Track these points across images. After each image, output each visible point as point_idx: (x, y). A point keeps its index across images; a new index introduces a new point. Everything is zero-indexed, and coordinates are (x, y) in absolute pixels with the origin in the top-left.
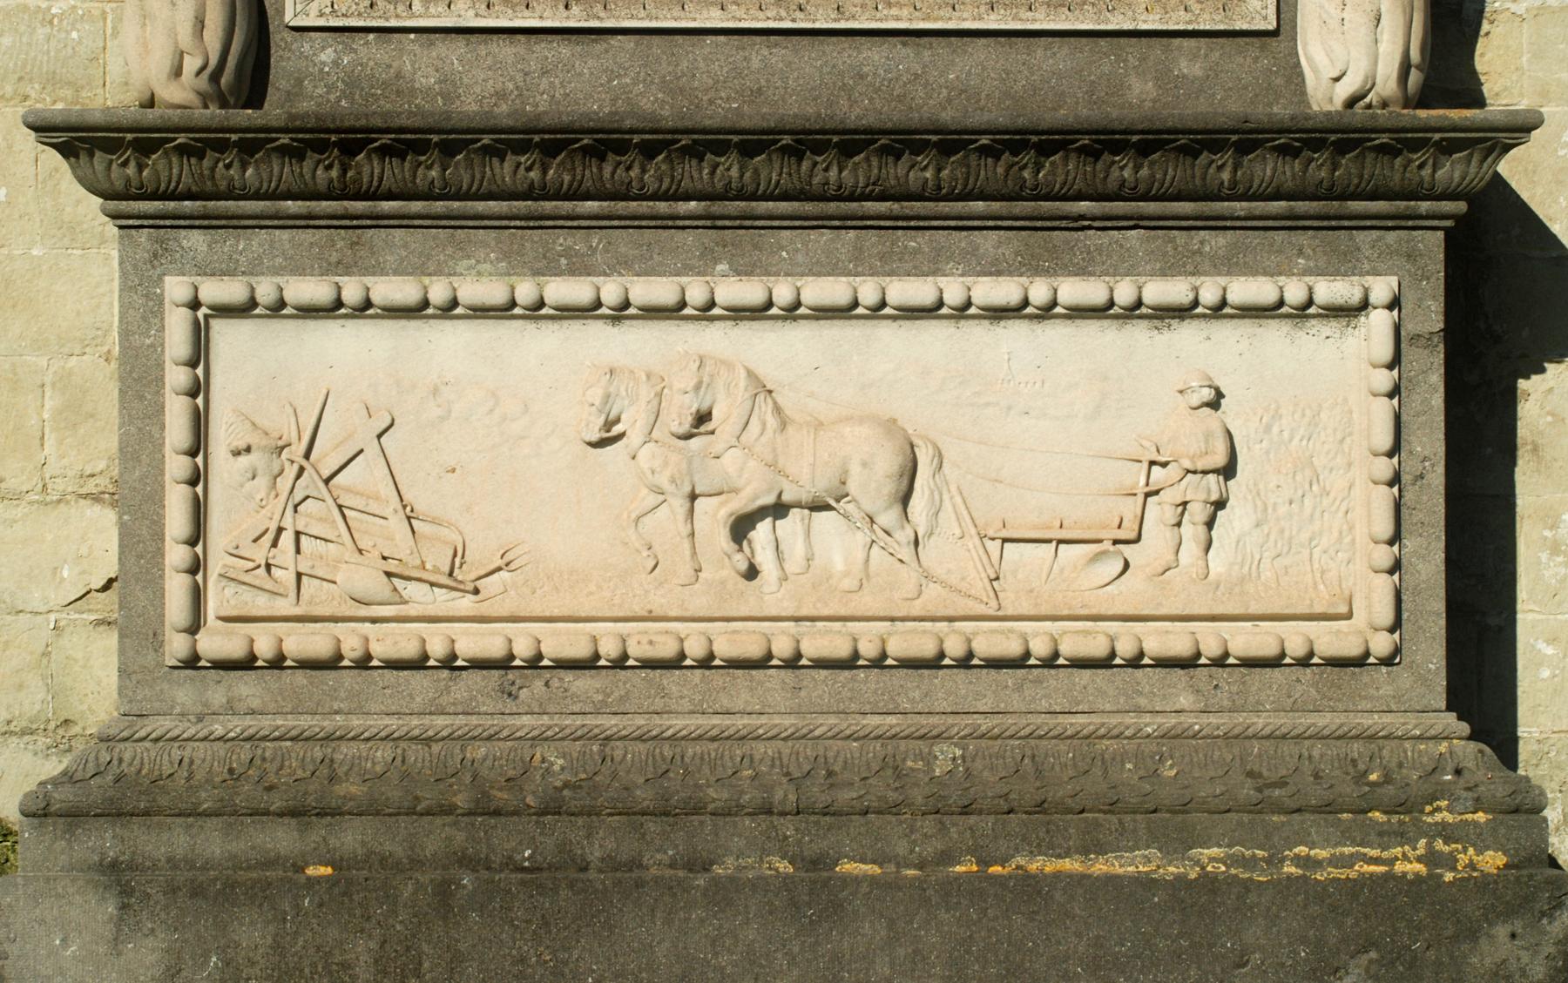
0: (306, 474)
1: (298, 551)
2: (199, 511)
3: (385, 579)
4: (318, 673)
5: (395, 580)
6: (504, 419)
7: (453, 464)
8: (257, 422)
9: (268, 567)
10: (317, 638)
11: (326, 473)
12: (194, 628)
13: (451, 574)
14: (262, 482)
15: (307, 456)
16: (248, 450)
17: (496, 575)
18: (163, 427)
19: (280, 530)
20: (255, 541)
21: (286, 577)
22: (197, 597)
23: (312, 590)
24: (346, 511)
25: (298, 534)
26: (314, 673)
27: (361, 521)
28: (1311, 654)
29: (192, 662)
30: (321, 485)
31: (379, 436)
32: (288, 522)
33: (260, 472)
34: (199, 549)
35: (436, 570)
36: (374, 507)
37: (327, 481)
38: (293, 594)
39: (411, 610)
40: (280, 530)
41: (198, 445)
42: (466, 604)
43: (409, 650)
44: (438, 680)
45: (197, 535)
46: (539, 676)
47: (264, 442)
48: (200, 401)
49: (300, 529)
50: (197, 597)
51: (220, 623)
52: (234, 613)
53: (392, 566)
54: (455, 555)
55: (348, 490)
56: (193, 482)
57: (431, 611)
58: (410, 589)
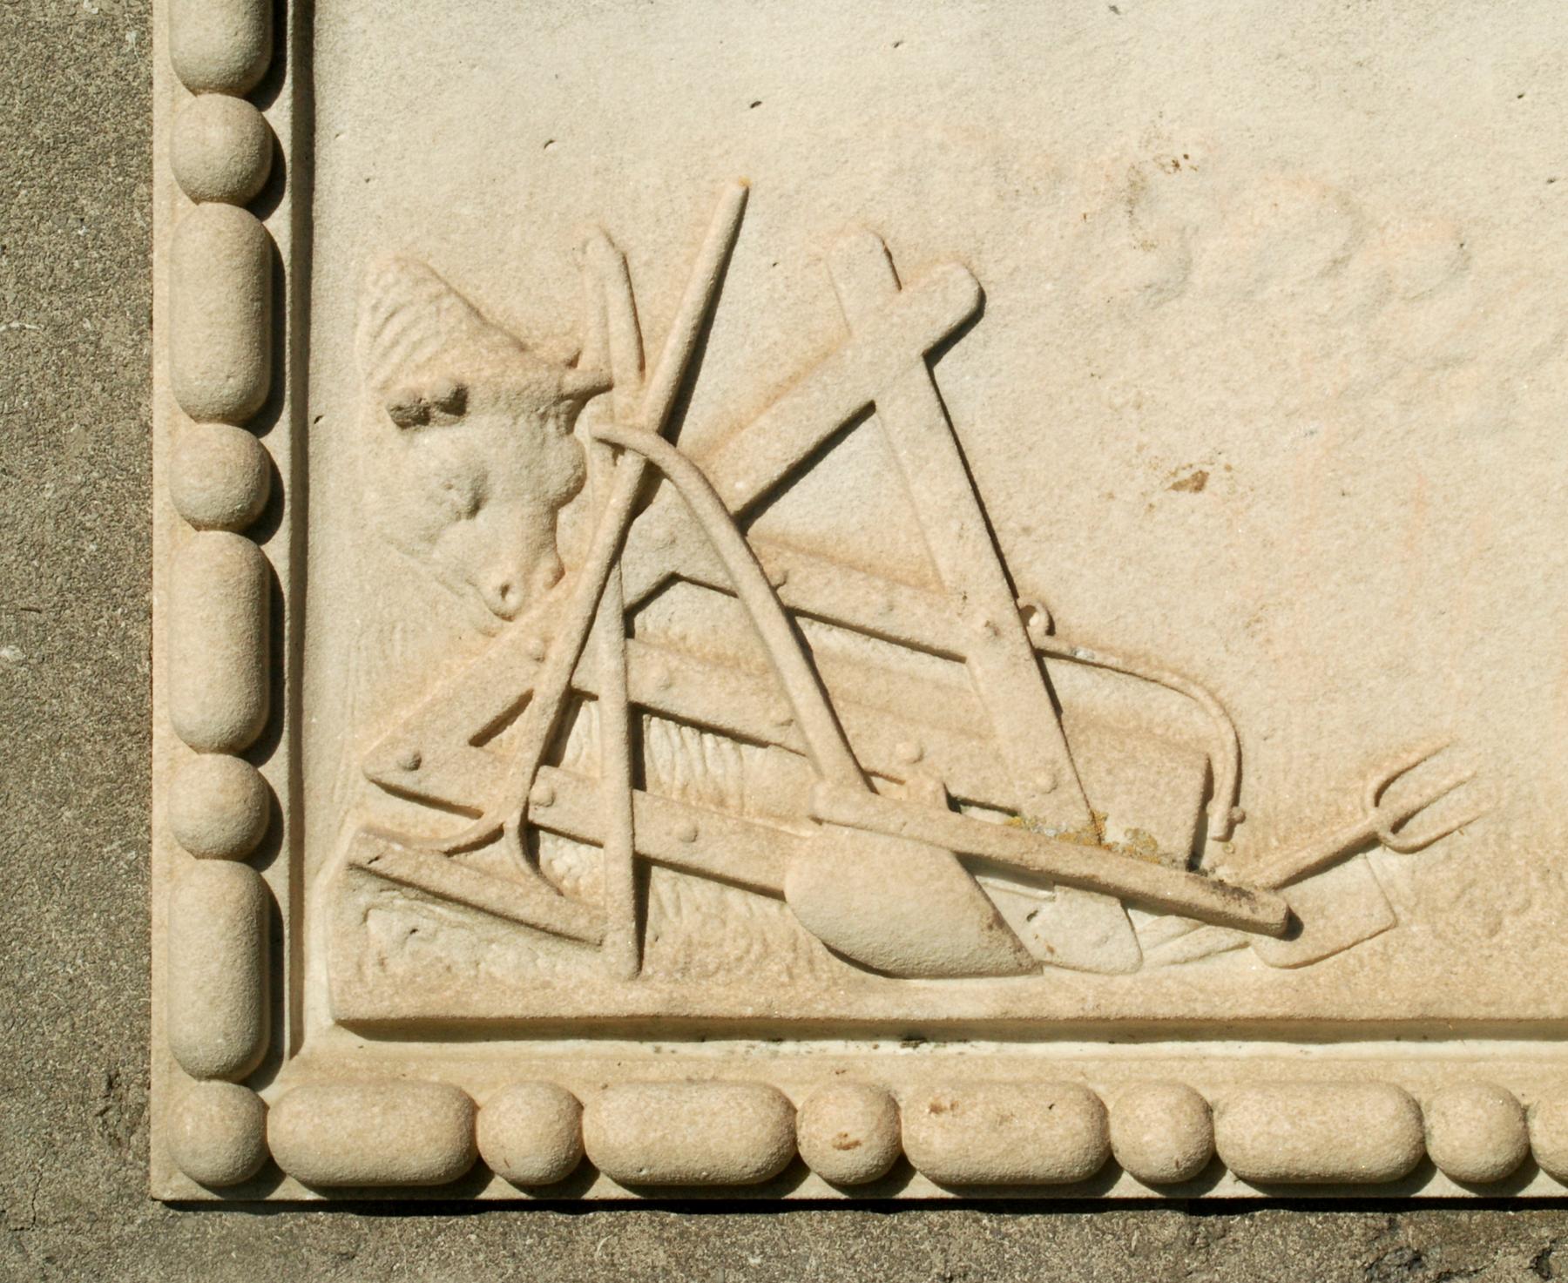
0: (665, 494)
1: (637, 779)
2: (276, 630)
3: (963, 883)
4: (708, 1224)
5: (995, 886)
6: (1383, 292)
7: (1196, 457)
8: (489, 301)
9: (530, 834)
10: (713, 1099)
11: (741, 492)
12: (256, 1065)
13: (1193, 864)
14: (506, 522)
15: (670, 427)
16: (457, 404)
17: (1356, 864)
18: (144, 321)
19: (572, 700)
20: (480, 740)
21: (594, 873)
22: (271, 943)
23: (689, 921)
24: (815, 633)
25: (636, 713)
26: (691, 1223)
27: (866, 667)
28: (1526, 1165)
29: (252, 1183)
30: (724, 533)
31: (932, 356)
32: (600, 672)
33: (497, 488)
34: (276, 770)
35: (1143, 848)
36: (915, 619)
37: (743, 520)
38: (621, 937)
39: (1057, 995)
40: (572, 700)
41: (273, 386)
42: (1250, 974)
43: (1050, 1145)
44: (1145, 1251)
45: (268, 721)
46: (1515, 1234)
47: (516, 377)
48: (280, 223)
49: (646, 696)
50: (271, 943)
51: (354, 1040)
52: (407, 1006)
53: (984, 833)
54: (1208, 794)
55: (817, 553)
56: (255, 523)
57: (1130, 998)
58: (1054, 920)
